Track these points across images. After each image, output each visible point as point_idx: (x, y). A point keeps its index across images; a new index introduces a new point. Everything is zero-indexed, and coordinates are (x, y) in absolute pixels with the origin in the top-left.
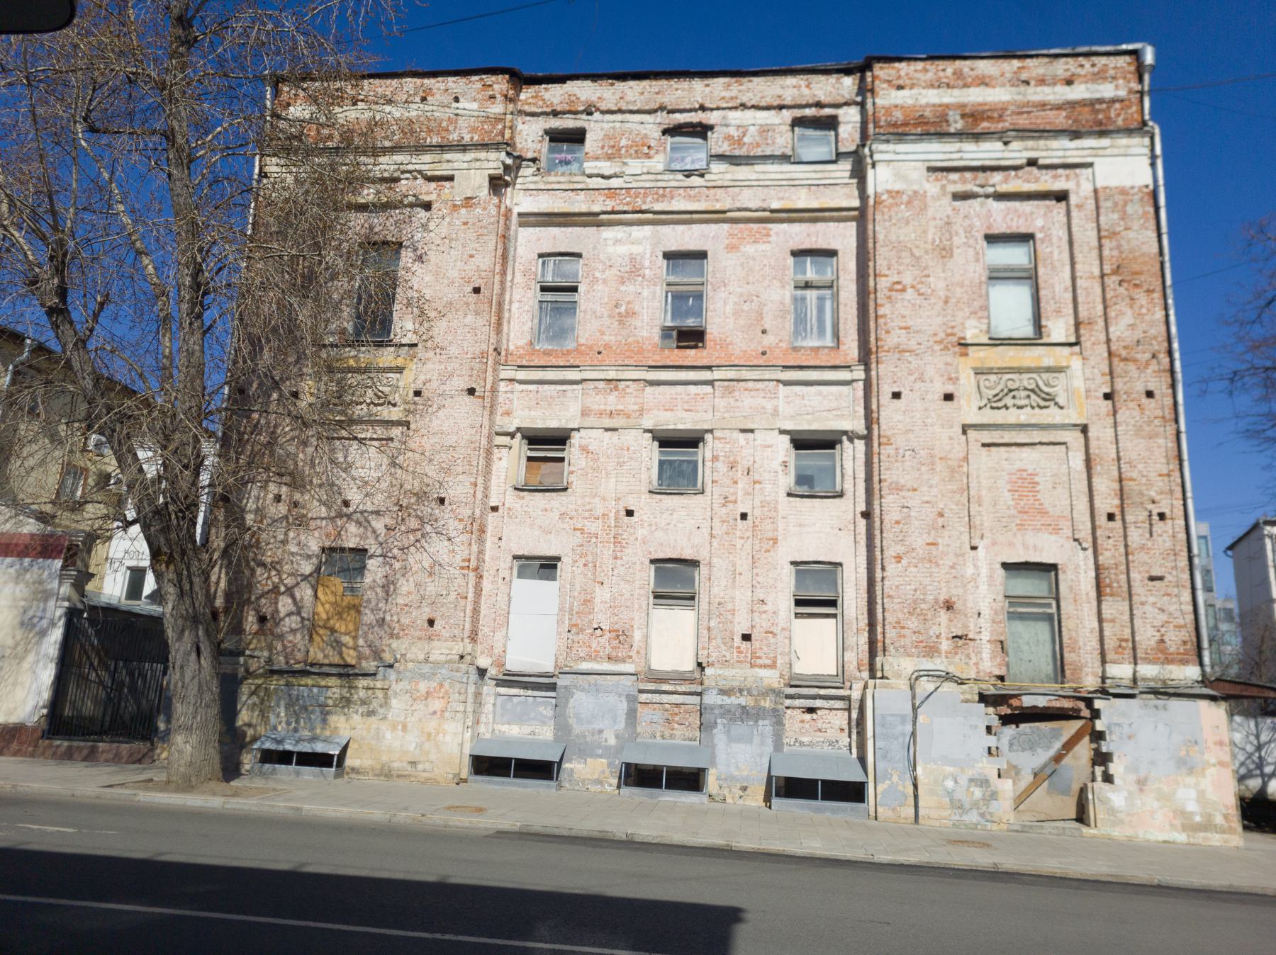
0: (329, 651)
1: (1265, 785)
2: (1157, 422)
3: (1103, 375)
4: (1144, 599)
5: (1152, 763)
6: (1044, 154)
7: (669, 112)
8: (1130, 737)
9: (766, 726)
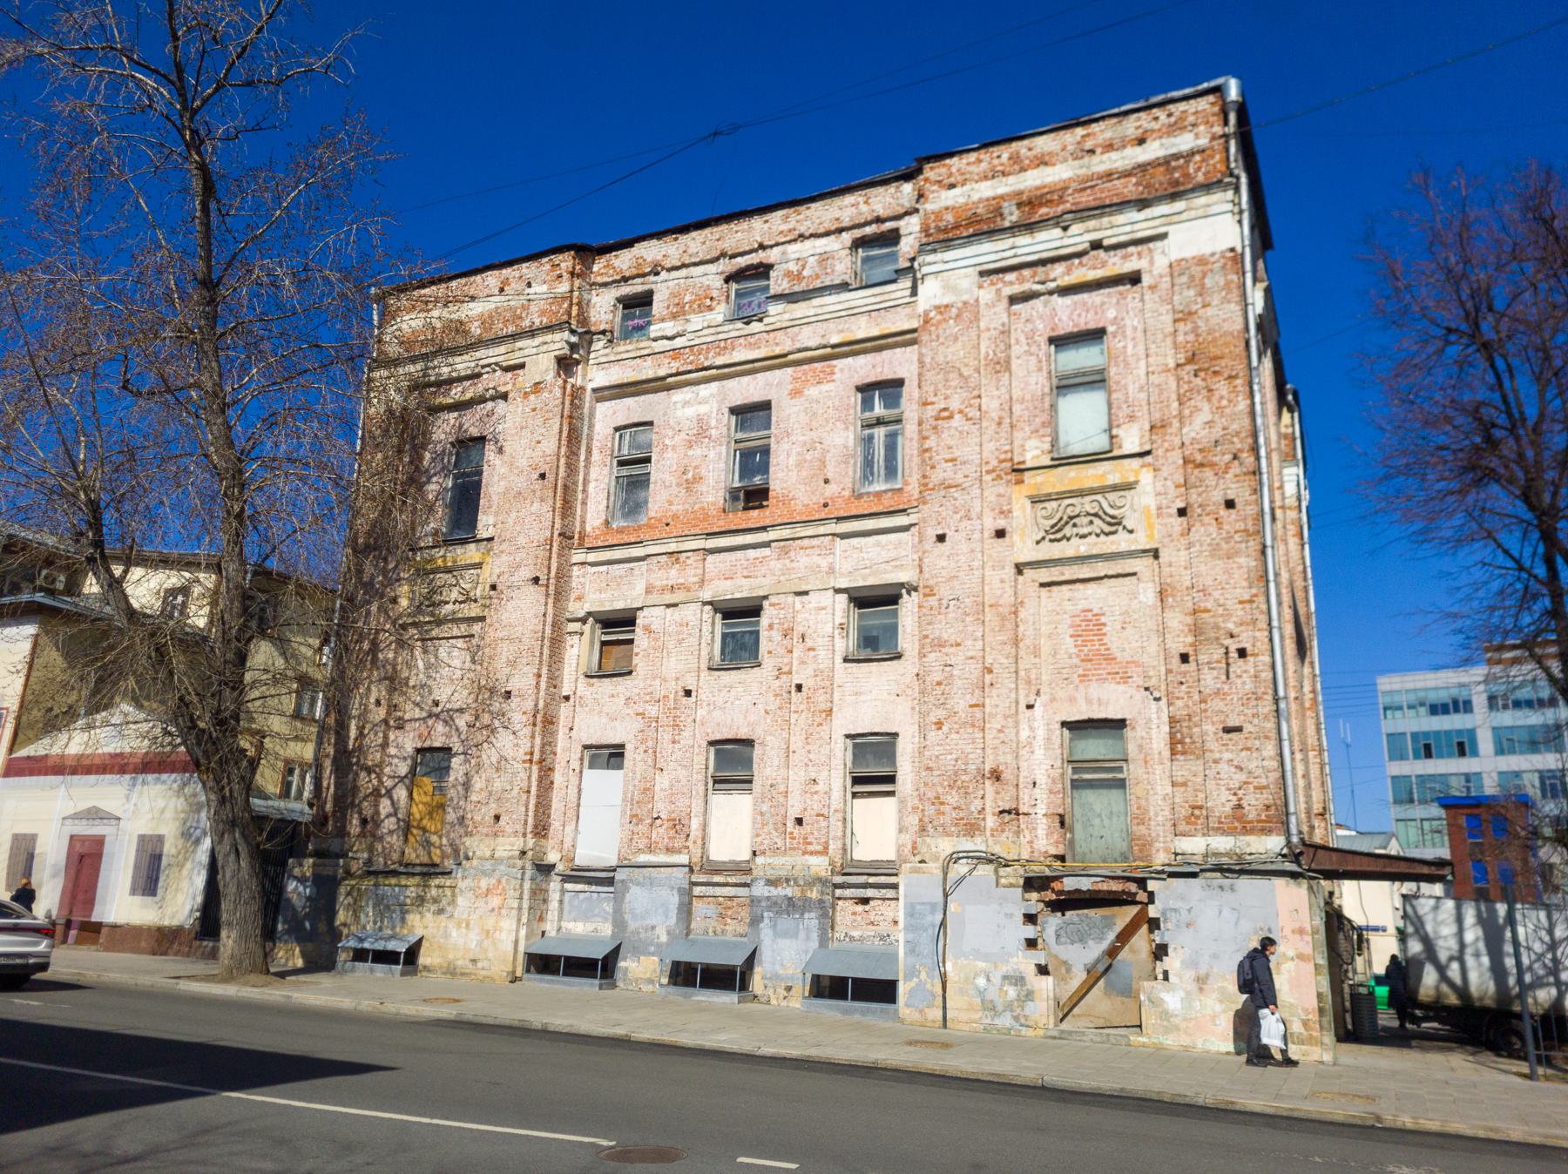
0: (421, 852)
1: (1561, 996)
2: (1237, 537)
3: (1177, 486)
4: (1217, 756)
5: (1215, 956)
6: (1109, 233)
7: (733, 256)
8: (1188, 925)
9: (811, 920)
